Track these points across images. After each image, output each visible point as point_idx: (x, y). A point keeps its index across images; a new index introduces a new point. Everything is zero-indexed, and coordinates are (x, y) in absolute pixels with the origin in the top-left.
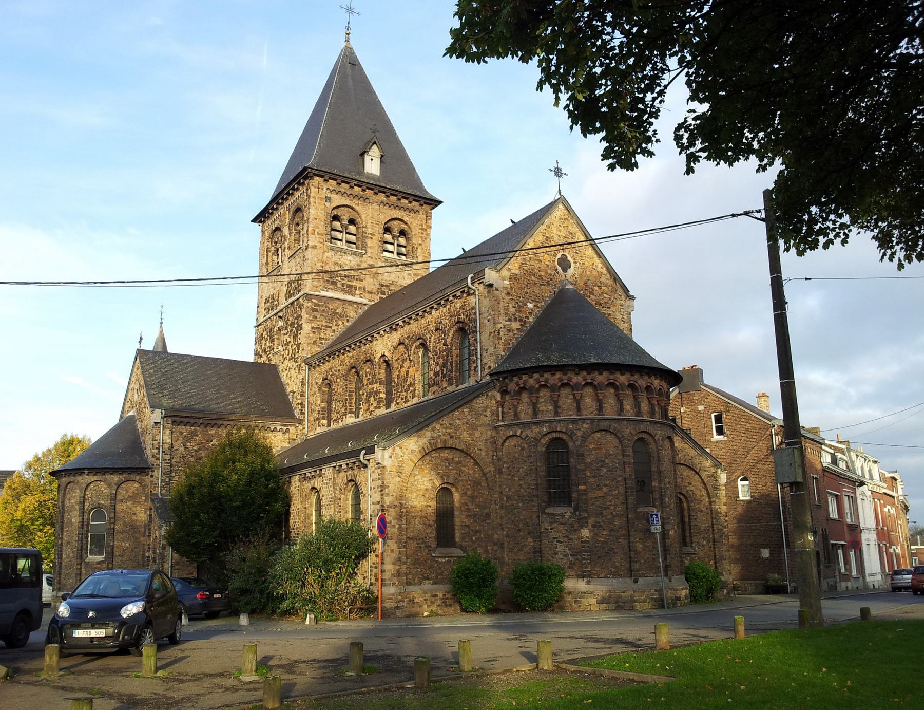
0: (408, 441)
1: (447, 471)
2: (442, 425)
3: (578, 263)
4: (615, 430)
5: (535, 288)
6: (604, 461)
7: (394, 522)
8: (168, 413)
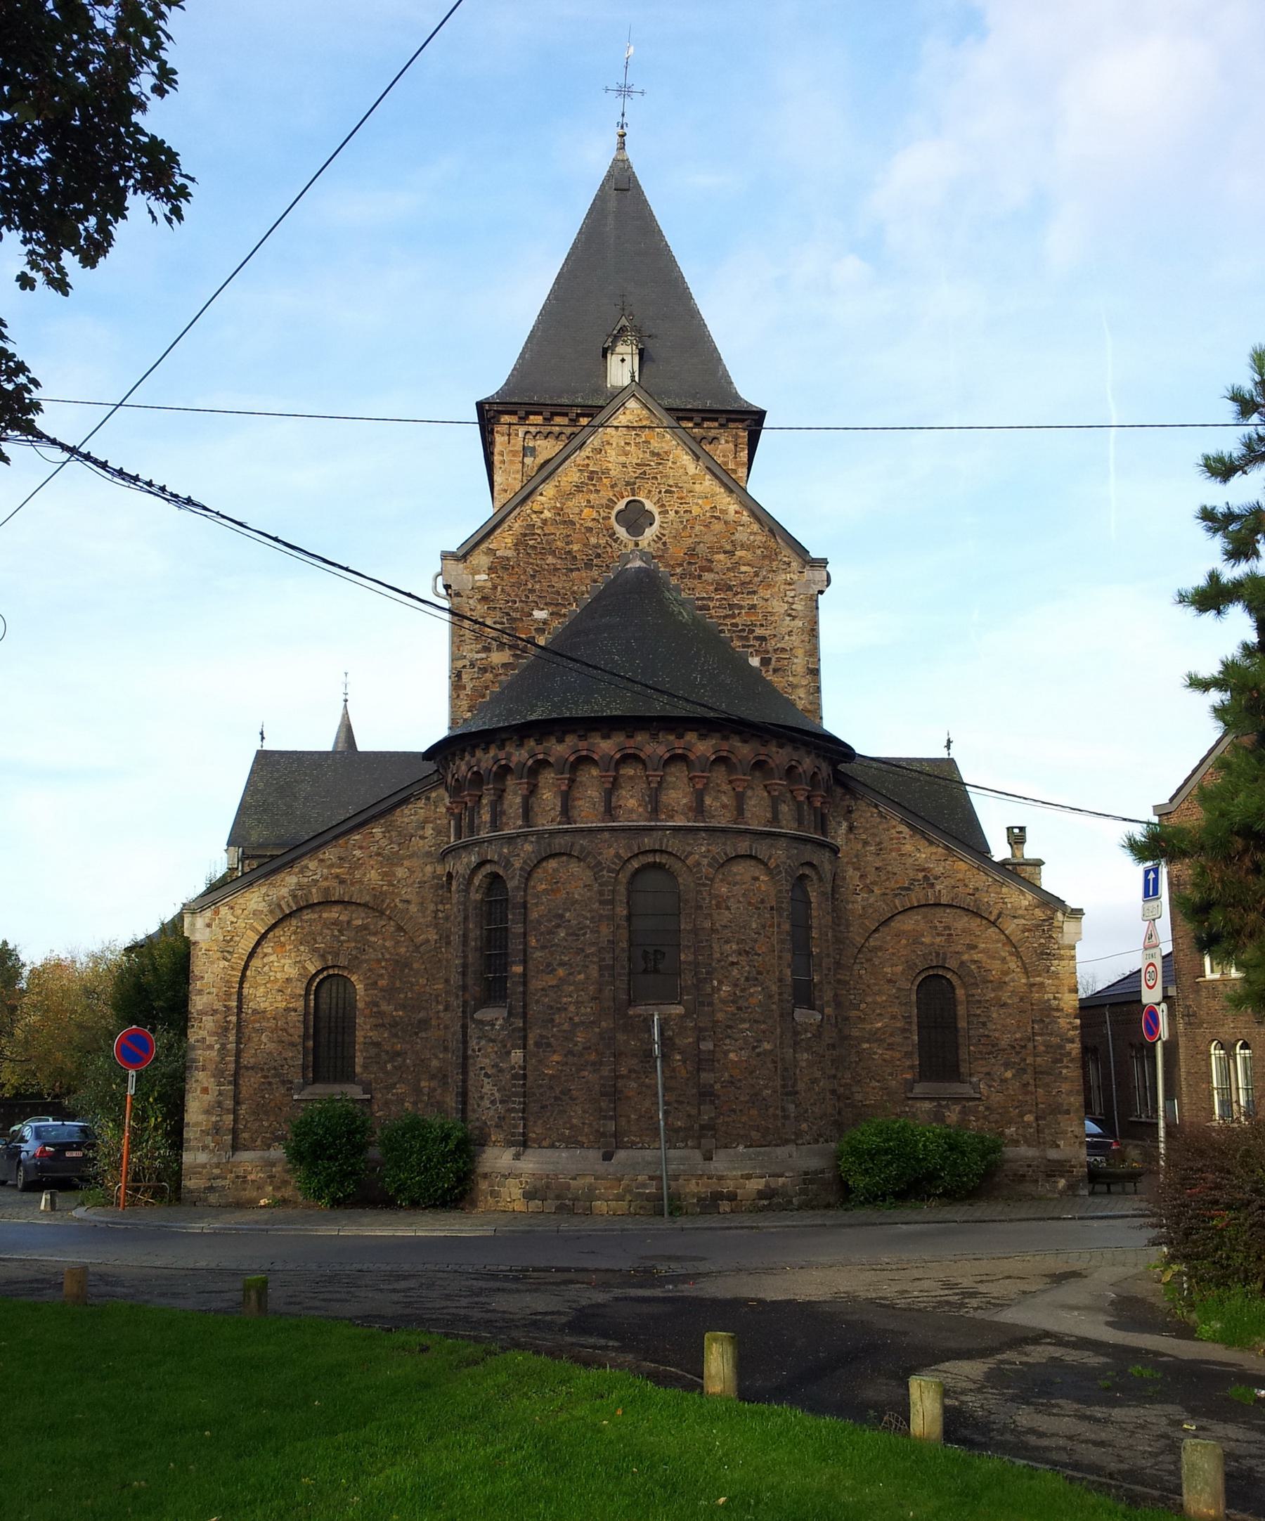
0: (247, 894)
1: (336, 945)
2: (322, 861)
3: (672, 513)
4: (581, 852)
5: (555, 579)
6: (562, 916)
7: (210, 1040)
8: (249, 852)
